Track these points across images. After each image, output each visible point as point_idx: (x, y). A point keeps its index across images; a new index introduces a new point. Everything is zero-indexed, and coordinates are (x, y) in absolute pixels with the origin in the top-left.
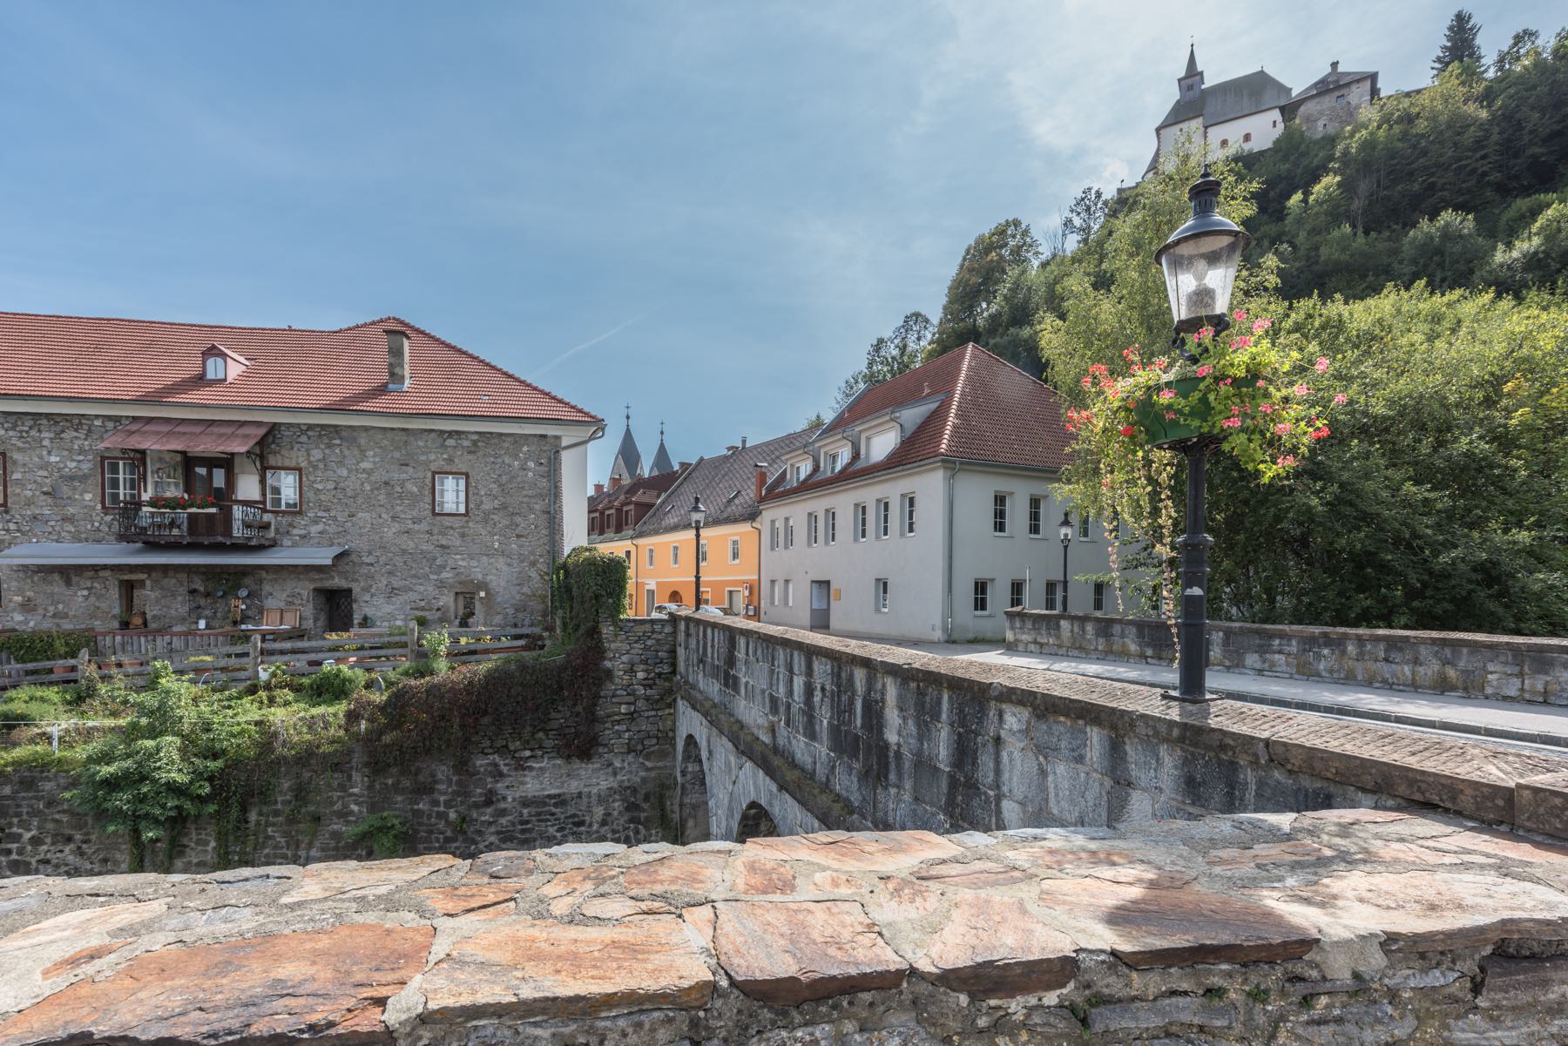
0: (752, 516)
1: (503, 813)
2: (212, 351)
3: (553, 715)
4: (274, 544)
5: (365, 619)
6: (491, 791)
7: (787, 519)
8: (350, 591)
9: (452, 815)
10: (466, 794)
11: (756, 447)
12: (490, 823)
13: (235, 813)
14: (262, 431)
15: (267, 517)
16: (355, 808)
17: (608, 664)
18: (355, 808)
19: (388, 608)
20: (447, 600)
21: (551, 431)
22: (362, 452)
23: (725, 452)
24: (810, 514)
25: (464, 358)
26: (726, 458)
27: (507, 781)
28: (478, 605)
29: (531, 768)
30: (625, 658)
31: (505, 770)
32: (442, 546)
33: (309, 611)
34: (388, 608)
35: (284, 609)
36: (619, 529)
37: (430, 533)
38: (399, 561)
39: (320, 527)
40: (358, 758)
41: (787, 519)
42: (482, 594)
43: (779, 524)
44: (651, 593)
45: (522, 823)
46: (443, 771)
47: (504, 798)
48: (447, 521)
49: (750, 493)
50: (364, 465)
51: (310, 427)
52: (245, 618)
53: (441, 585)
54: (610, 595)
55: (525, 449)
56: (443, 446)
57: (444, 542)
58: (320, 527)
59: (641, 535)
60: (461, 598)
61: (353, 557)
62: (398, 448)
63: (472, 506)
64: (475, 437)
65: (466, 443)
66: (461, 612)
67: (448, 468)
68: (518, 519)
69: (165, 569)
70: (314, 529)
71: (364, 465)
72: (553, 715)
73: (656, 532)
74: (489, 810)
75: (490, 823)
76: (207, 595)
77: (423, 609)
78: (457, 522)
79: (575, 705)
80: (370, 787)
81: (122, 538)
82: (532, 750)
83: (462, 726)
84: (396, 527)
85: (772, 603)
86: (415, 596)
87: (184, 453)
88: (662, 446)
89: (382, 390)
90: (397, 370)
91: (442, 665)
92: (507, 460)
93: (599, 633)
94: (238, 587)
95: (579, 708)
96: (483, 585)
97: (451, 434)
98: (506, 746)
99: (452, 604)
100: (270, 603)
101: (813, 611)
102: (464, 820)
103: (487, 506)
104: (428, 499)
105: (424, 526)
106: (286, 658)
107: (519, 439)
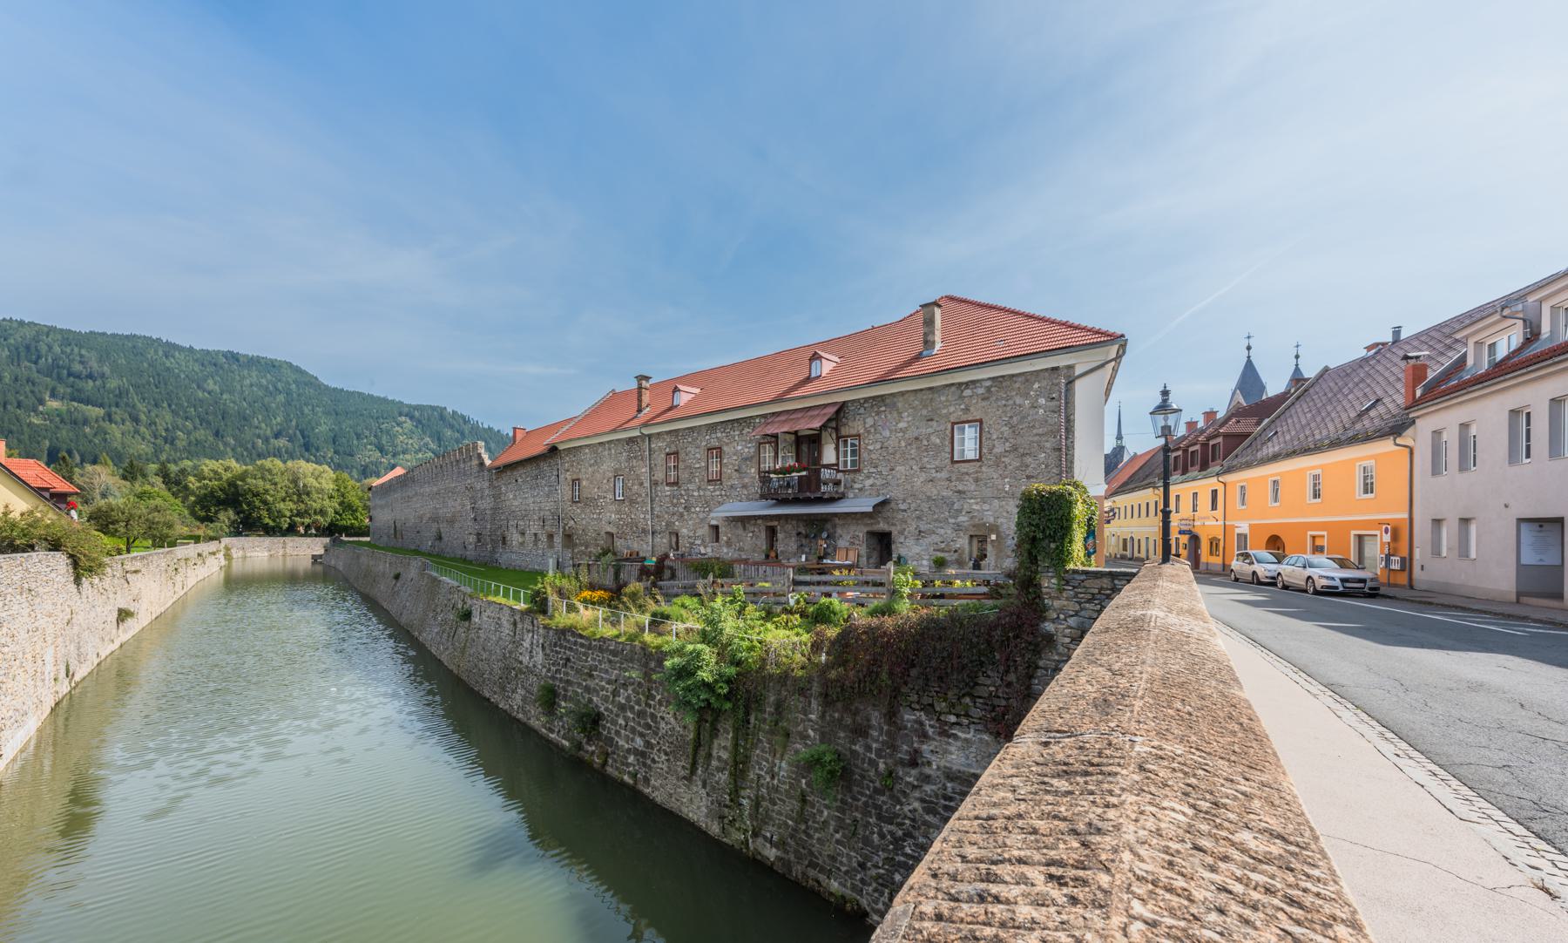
0: (1396, 429)
1: (927, 779)
2: (815, 357)
3: (981, 680)
4: (842, 497)
5: (899, 558)
6: (916, 751)
7: (1465, 426)
8: (889, 534)
9: (882, 766)
10: (894, 748)
11: (1417, 336)
12: (915, 787)
13: (741, 714)
14: (833, 410)
15: (840, 476)
16: (811, 733)
17: (1049, 627)
18: (811, 733)
19: (917, 549)
20: (962, 542)
21: (1061, 361)
22: (900, 413)
23: (1363, 353)
24: (1514, 413)
25: (993, 312)
26: (1365, 360)
27: (932, 745)
28: (989, 548)
29: (955, 737)
30: (1072, 621)
31: (931, 731)
32: (959, 492)
33: (863, 550)
34: (917, 549)
35: (850, 547)
36: (1204, 466)
37: (949, 480)
38: (925, 506)
39: (870, 481)
40: (816, 688)
41: (1465, 426)
42: (993, 537)
43: (1451, 437)
44: (1242, 538)
45: (946, 798)
46: (876, 717)
47: (929, 763)
48: (964, 468)
49: (1397, 399)
50: (902, 425)
51: (866, 400)
52: (826, 555)
53: (958, 528)
54: (1052, 538)
55: (1036, 386)
56: (961, 397)
57: (960, 488)
58: (870, 481)
59: (1229, 470)
60: (975, 541)
61: (893, 505)
62: (925, 406)
63: (985, 451)
64: (988, 383)
65: (980, 391)
66: (975, 554)
67: (964, 418)
68: (1029, 460)
69: (787, 517)
70: (868, 482)
71: (902, 425)
72: (981, 680)
73: (1248, 465)
74: (914, 772)
75: (915, 787)
76: (807, 536)
77: (942, 550)
78: (970, 468)
79: (1007, 672)
80: (822, 717)
81: (763, 497)
82: (958, 716)
83: (891, 674)
84: (923, 477)
85: (1436, 551)
86: (936, 539)
87: (796, 433)
88: (1249, 365)
89: (918, 357)
90: (930, 338)
91: (904, 607)
92: (1018, 400)
93: (1038, 586)
94: (821, 530)
95: (1012, 677)
96: (994, 528)
97: (967, 384)
98: (932, 705)
99: (967, 547)
100: (842, 543)
101: (1520, 567)
102: (890, 773)
103: (999, 449)
104: (948, 449)
105: (944, 475)
106: (807, 588)
107: (1028, 377)
